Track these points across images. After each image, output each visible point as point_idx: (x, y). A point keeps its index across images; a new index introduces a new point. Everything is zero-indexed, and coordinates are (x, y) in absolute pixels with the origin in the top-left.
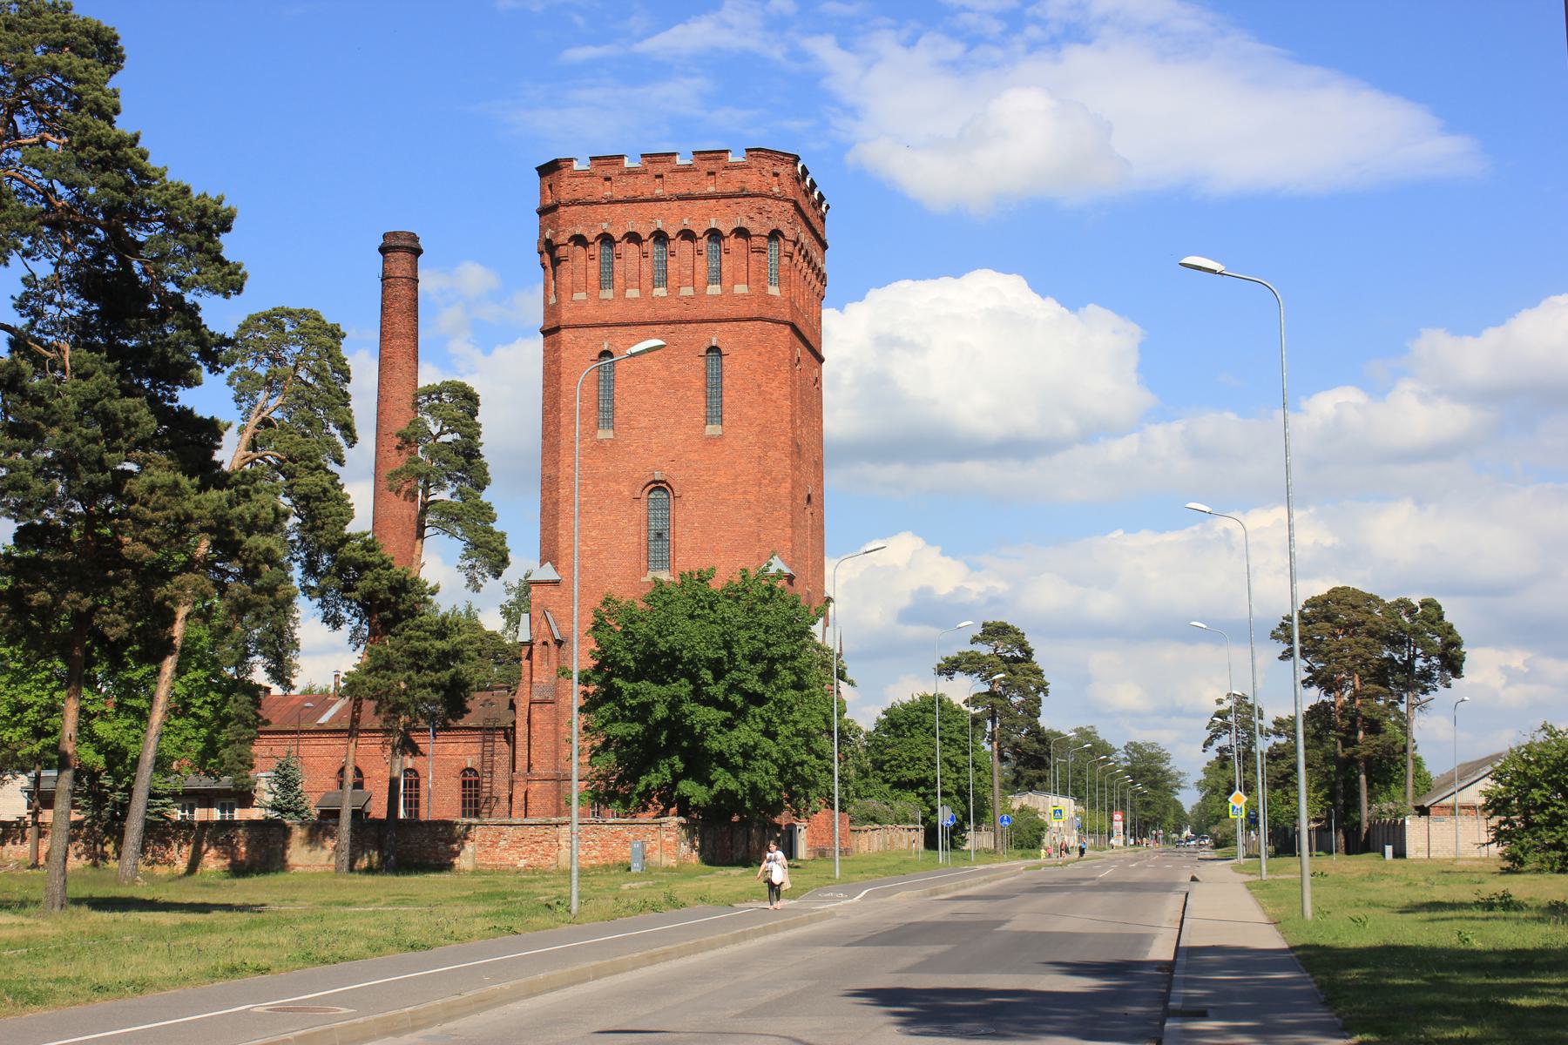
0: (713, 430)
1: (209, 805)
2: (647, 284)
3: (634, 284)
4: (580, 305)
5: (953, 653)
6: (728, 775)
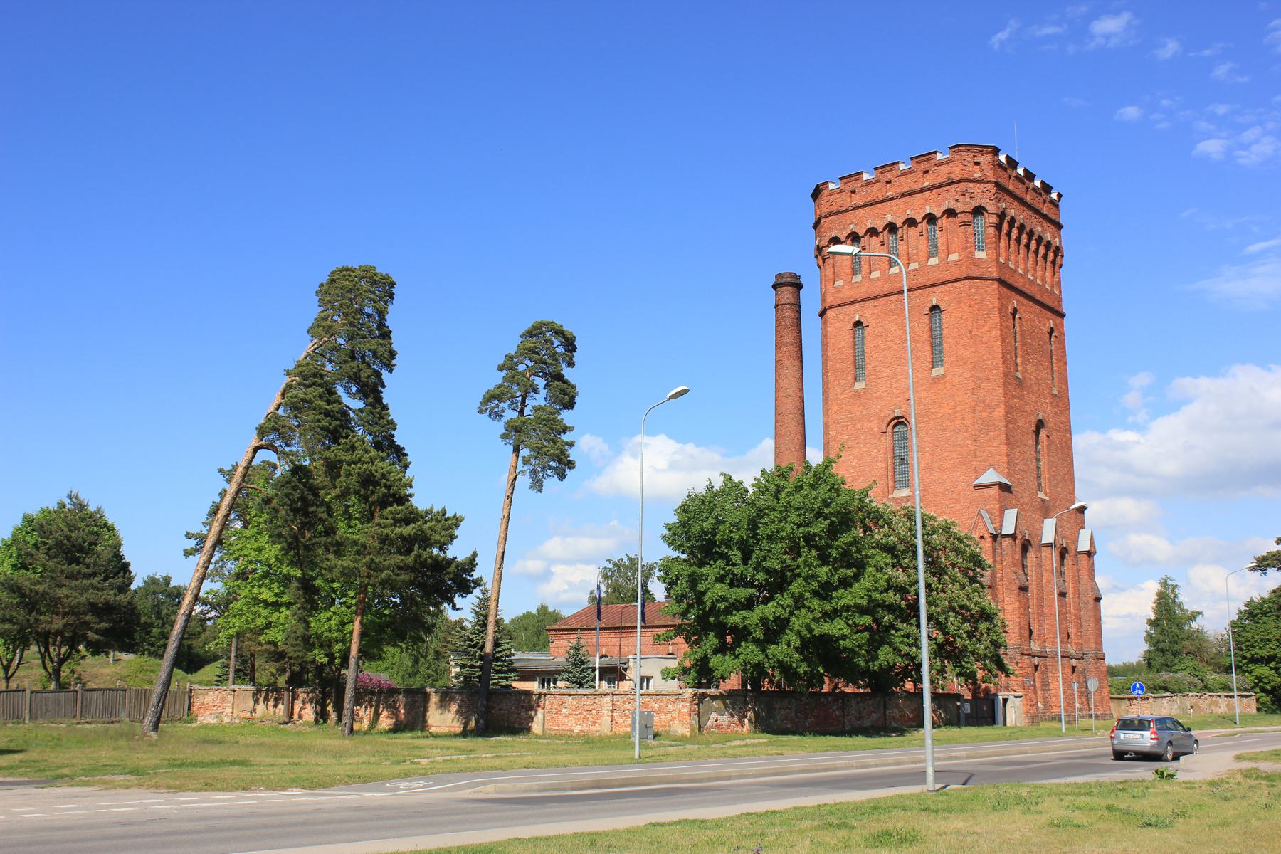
0: (937, 372)
4: (839, 290)
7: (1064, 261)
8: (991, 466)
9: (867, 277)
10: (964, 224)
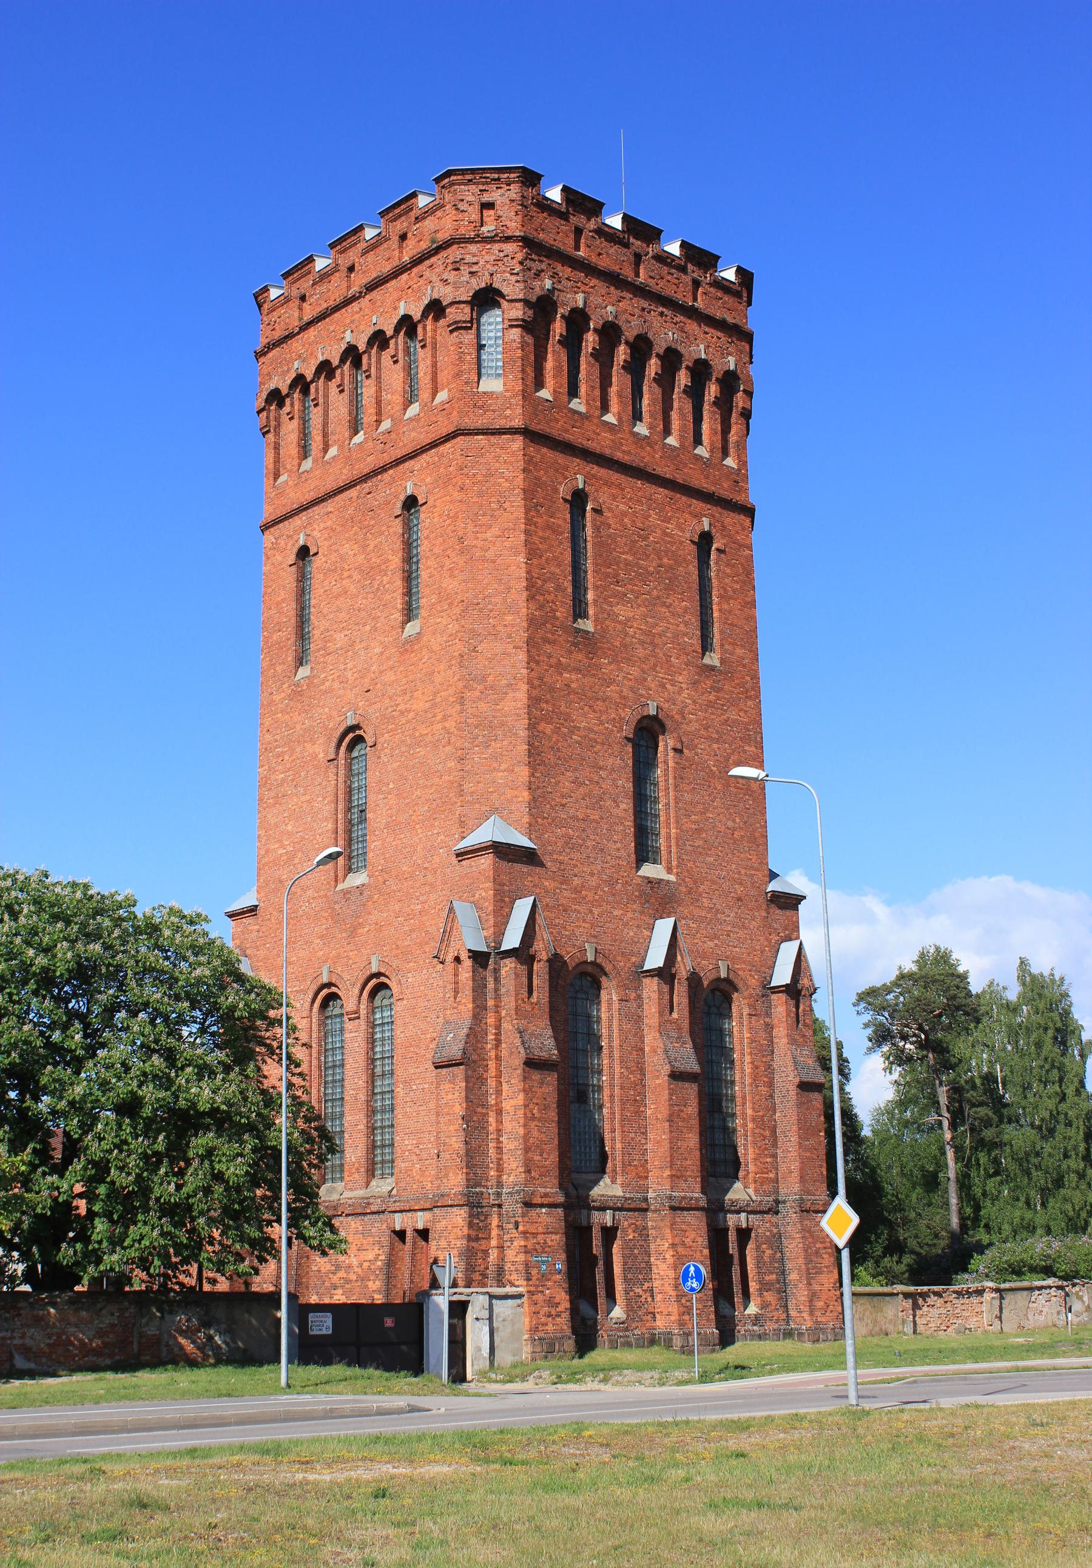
7: (758, 406)
8: (495, 810)
10: (457, 327)
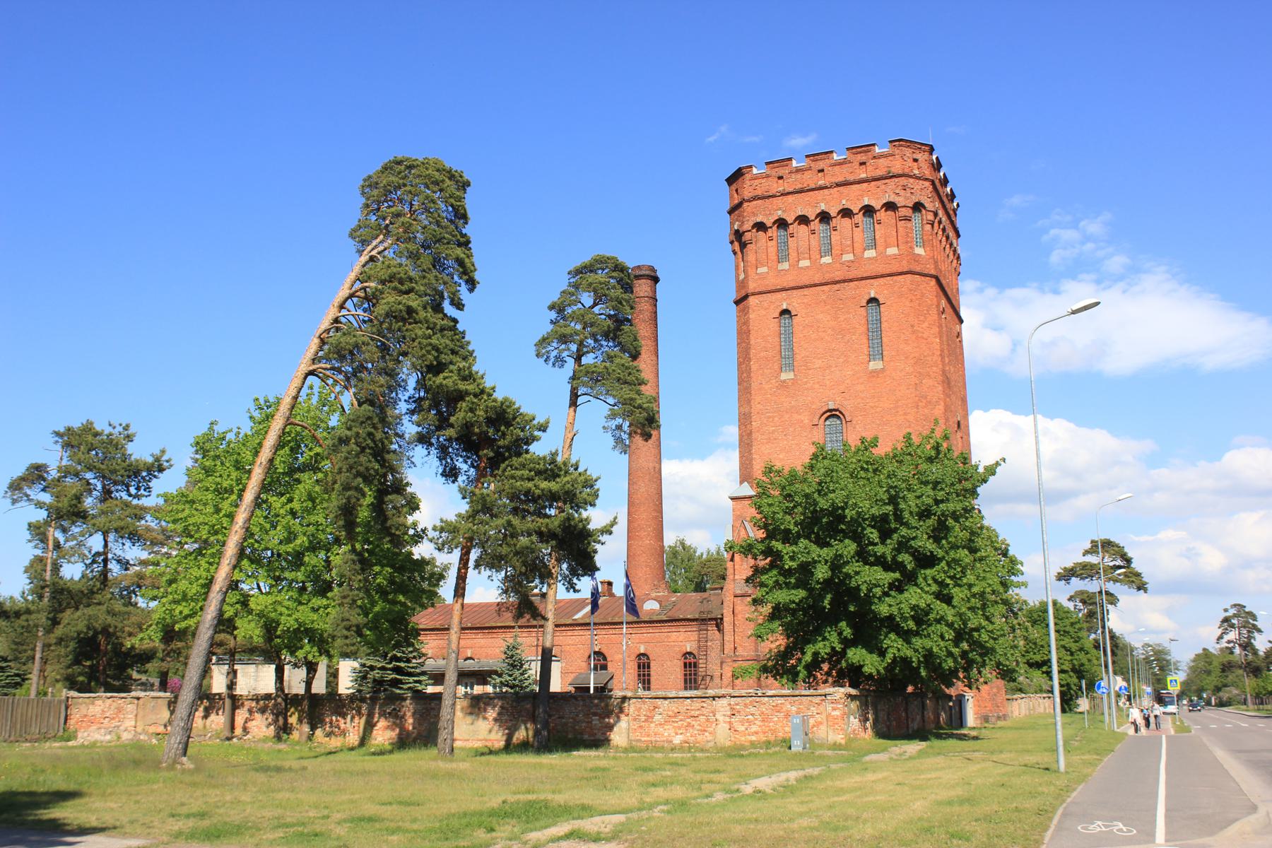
0: (875, 365)
1: (485, 683)
2: (815, 255)
3: (806, 255)
5: (1069, 565)
6: (900, 641)
9: (794, 266)
